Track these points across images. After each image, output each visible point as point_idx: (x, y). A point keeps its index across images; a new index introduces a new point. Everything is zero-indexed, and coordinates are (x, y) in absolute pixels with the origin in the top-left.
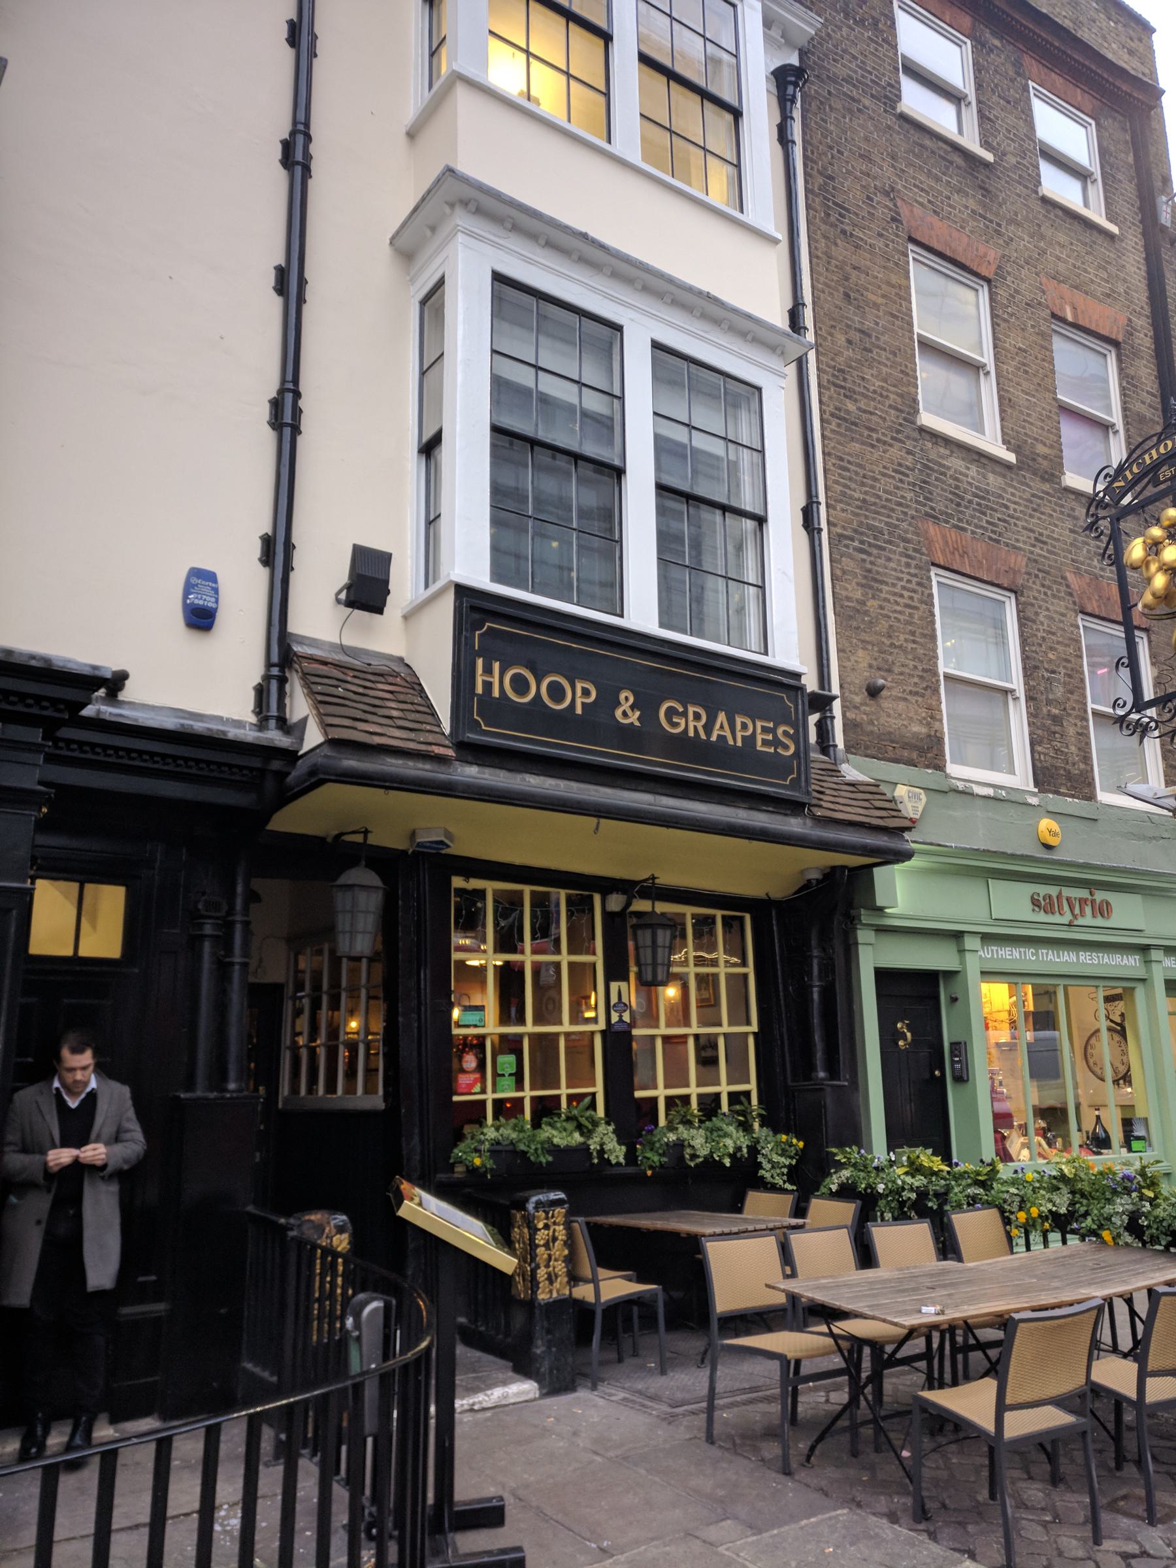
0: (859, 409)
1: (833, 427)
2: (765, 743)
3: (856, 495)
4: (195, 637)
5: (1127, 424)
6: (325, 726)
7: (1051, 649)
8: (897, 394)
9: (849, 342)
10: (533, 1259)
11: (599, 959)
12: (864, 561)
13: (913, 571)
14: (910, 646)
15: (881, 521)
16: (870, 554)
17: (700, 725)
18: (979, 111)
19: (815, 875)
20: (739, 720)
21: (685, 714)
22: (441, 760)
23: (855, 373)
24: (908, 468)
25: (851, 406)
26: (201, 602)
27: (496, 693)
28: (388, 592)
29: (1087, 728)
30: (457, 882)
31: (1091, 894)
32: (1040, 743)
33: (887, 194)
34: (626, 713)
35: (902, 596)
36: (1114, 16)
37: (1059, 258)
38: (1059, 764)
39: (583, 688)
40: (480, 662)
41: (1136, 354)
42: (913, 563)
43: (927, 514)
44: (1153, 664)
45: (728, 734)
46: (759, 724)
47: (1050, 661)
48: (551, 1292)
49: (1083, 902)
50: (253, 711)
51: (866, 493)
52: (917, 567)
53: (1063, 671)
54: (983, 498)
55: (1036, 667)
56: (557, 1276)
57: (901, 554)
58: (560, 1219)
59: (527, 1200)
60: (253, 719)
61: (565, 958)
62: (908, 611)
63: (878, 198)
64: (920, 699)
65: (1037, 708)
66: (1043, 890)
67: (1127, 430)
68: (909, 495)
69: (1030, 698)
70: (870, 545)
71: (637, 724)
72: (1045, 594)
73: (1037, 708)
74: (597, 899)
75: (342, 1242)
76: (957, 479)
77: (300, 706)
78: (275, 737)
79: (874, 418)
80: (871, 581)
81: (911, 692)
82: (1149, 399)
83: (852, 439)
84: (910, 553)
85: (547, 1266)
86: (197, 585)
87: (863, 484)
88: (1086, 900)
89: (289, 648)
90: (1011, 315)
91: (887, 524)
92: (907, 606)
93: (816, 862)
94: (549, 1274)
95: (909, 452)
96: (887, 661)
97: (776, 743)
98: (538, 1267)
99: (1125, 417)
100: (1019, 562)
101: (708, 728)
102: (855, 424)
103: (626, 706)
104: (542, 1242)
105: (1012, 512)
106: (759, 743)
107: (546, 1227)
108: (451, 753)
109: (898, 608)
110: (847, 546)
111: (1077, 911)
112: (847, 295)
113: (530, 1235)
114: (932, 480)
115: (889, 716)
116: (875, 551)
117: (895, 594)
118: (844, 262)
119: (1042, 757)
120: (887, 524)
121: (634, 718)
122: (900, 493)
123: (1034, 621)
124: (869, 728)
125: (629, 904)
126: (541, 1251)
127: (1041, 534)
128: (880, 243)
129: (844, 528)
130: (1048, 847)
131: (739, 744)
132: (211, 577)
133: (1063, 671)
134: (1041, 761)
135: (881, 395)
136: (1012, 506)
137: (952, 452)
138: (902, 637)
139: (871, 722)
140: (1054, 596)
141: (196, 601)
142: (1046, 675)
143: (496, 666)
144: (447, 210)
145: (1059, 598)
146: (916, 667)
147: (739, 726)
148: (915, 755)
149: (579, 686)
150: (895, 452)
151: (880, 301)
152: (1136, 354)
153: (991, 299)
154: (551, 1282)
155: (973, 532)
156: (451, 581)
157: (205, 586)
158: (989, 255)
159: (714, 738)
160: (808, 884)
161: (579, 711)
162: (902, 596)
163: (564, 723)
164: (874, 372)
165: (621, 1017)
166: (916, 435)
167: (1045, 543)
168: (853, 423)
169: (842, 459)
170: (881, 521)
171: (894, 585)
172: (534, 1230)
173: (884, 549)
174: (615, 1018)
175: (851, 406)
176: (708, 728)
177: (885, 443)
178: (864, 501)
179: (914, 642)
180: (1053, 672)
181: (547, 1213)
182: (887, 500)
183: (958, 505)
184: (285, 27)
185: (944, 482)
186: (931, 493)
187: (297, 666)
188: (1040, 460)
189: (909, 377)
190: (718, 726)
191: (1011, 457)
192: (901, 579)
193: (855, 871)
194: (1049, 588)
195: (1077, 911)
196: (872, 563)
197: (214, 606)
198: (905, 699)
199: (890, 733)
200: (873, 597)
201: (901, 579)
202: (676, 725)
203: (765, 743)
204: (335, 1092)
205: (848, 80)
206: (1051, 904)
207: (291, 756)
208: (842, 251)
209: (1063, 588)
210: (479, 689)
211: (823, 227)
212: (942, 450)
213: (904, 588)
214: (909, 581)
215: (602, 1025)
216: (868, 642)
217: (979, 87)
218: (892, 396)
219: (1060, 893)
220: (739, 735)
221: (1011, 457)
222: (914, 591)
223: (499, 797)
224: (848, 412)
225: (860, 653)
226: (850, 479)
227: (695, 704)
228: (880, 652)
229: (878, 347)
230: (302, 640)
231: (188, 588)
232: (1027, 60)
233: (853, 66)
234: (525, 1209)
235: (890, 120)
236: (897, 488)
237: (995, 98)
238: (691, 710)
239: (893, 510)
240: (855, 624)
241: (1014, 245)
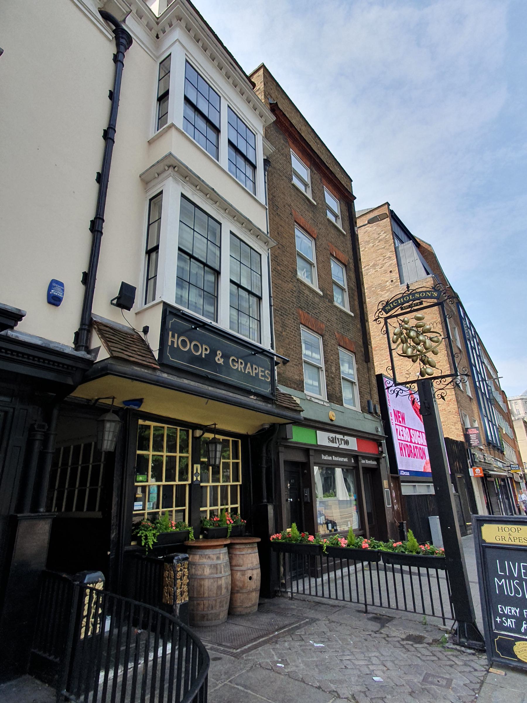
0: (281, 269)
1: (274, 274)
3: (280, 297)
5: (349, 289)
6: (110, 350)
7: (332, 355)
9: (279, 248)
10: (175, 585)
11: (190, 455)
12: (282, 319)
13: (296, 324)
14: (295, 349)
15: (287, 307)
16: (284, 317)
18: (312, 190)
19: (267, 426)
20: (254, 366)
21: (237, 362)
22: (154, 369)
23: (280, 258)
24: (294, 291)
25: (279, 268)
26: (56, 294)
27: (175, 346)
28: (134, 302)
29: (341, 382)
30: (141, 422)
32: (329, 386)
33: (289, 206)
35: (292, 332)
37: (332, 237)
38: (334, 393)
39: (205, 348)
40: (170, 333)
41: (350, 270)
42: (295, 322)
44: (356, 364)
45: (250, 371)
46: (260, 369)
47: (331, 359)
48: (181, 600)
49: (341, 439)
50: (74, 343)
51: (283, 296)
52: (296, 323)
54: (314, 305)
56: (184, 592)
57: (292, 318)
59: (173, 558)
60: (73, 346)
61: (178, 455)
62: (294, 337)
63: (287, 206)
65: (328, 374)
66: (333, 435)
67: (349, 292)
68: (295, 300)
69: (326, 371)
71: (222, 364)
73: (328, 374)
74: (190, 431)
75: (100, 586)
76: (307, 297)
77: (96, 341)
78: (81, 354)
79: (285, 273)
80: (284, 326)
81: (295, 365)
82: (354, 283)
83: (279, 279)
84: (295, 318)
85: (181, 588)
86: (55, 286)
87: (282, 294)
89: (92, 319)
90: (321, 250)
91: (288, 308)
93: (267, 420)
94: (181, 592)
95: (295, 286)
96: (288, 353)
98: (177, 589)
99: (348, 287)
100: (323, 326)
101: (245, 368)
104: (179, 577)
106: (260, 376)
107: (181, 570)
109: (292, 336)
110: (277, 313)
111: (340, 443)
112: (278, 233)
113: (174, 574)
114: (301, 296)
115: (289, 372)
116: (285, 316)
117: (291, 331)
118: (278, 223)
120: (288, 308)
121: (221, 361)
122: (292, 299)
123: (327, 346)
124: (283, 375)
125: (203, 434)
126: (179, 581)
127: (329, 319)
128: (287, 220)
129: (276, 307)
130: (332, 420)
132: (62, 284)
136: (321, 308)
138: (292, 346)
139: (284, 373)
141: (54, 293)
143: (176, 335)
144: (167, 168)
145: (333, 339)
146: (296, 356)
147: (254, 369)
150: (290, 285)
151: (287, 237)
152: (350, 270)
153: (315, 245)
155: (311, 315)
156: (162, 301)
157: (58, 288)
158: (315, 231)
159: (246, 372)
160: (263, 429)
161: (203, 356)
162: (292, 332)
163: (198, 360)
165: (197, 478)
166: (296, 281)
167: (330, 322)
168: (280, 274)
169: (276, 285)
170: (287, 307)
171: (290, 328)
172: (176, 572)
173: (287, 316)
174: (195, 479)
176: (245, 368)
177: (288, 282)
178: (282, 299)
179: (296, 348)
180: (332, 363)
181: (181, 564)
183: (308, 305)
184: (108, 92)
185: (304, 297)
186: (300, 300)
187: (95, 326)
188: (328, 296)
189: (295, 262)
190: (248, 368)
191: (321, 293)
192: (292, 327)
193: (280, 425)
194: (331, 336)
195: (340, 443)
196: (284, 320)
197: (62, 296)
198: (293, 367)
199: (289, 378)
200: (285, 331)
201: (292, 327)
202: (235, 366)
203: (262, 376)
204: (82, 510)
205: (279, 170)
206: (333, 440)
207: (90, 363)
208: (277, 219)
209: (334, 337)
210: (170, 344)
211: (272, 211)
212: (303, 288)
213: (293, 329)
214: (294, 328)
215: (190, 482)
216: (283, 346)
217: (312, 183)
219: (336, 436)
220: (254, 372)
221: (321, 293)
222: (296, 331)
223: (178, 387)
224: (278, 270)
225: (281, 349)
226: (279, 291)
228: (286, 350)
229: (287, 251)
231: (51, 287)
232: (323, 180)
233: (281, 166)
234: (173, 562)
235: (290, 185)
237: (316, 187)
239: (290, 304)
240: (279, 339)
241: (321, 230)
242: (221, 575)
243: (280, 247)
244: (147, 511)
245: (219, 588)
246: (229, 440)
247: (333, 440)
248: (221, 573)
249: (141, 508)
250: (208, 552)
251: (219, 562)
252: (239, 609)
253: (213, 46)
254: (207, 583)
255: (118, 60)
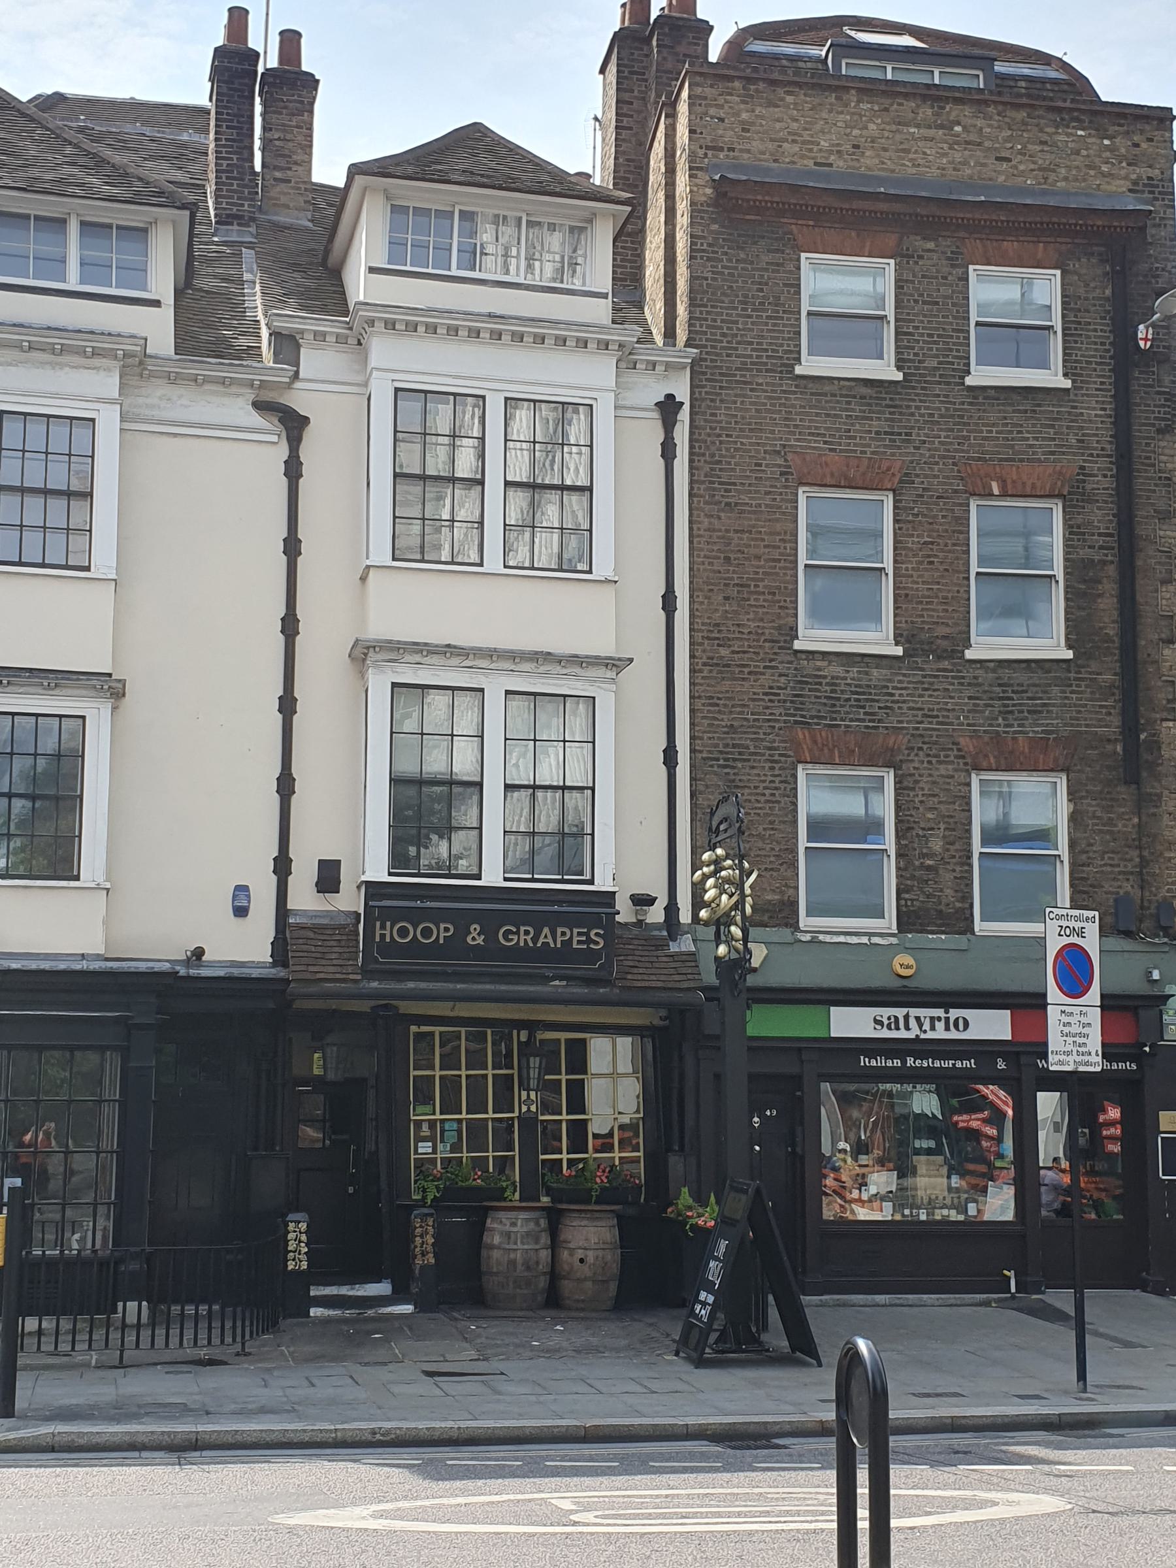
2: (579, 942)
4: (240, 920)
8: (773, 628)
16: (733, 768)
17: (529, 938)
20: (559, 930)
21: (518, 933)
30: (414, 1029)
31: (947, 1012)
34: (475, 937)
35: (764, 795)
36: (1113, 129)
38: (930, 905)
40: (378, 924)
42: (777, 766)
43: (796, 722)
44: (1069, 800)
45: (550, 940)
46: (575, 931)
53: (942, 826)
55: (910, 829)
58: (431, 1223)
60: (271, 960)
64: (775, 874)
70: (735, 760)
72: (929, 762)
83: (723, 679)
88: (939, 1019)
92: (768, 801)
97: (589, 941)
101: (535, 939)
102: (728, 666)
103: (474, 934)
105: (897, 698)
106: (575, 942)
107: (421, 1227)
108: (359, 977)
118: (727, 531)
119: (909, 903)
121: (480, 940)
131: (559, 946)
133: (942, 826)
134: (906, 906)
135: (757, 633)
137: (830, 662)
140: (940, 762)
142: (921, 833)
143: (388, 924)
147: (559, 934)
148: (766, 918)
149: (442, 926)
154: (423, 1255)
157: (242, 894)
161: (441, 941)
162: (764, 795)
163: (434, 951)
164: (751, 616)
174: (524, 1109)
175: (724, 652)
176: (535, 939)
182: (755, 720)
202: (512, 940)
210: (377, 939)
215: (516, 1114)
218: (767, 631)
220: (559, 940)
227: (524, 925)
230: (296, 913)
231: (234, 897)
236: (767, 708)
238: (522, 929)
242: (515, 1247)
243: (733, 592)
244: (439, 1156)
245: (513, 1263)
246: (415, 1077)
247: (894, 1024)
248: (516, 1243)
249: (430, 1150)
250: (502, 1214)
251: (515, 1229)
252: (567, 1302)
253: (444, 318)
254: (496, 1254)
255: (293, 470)
